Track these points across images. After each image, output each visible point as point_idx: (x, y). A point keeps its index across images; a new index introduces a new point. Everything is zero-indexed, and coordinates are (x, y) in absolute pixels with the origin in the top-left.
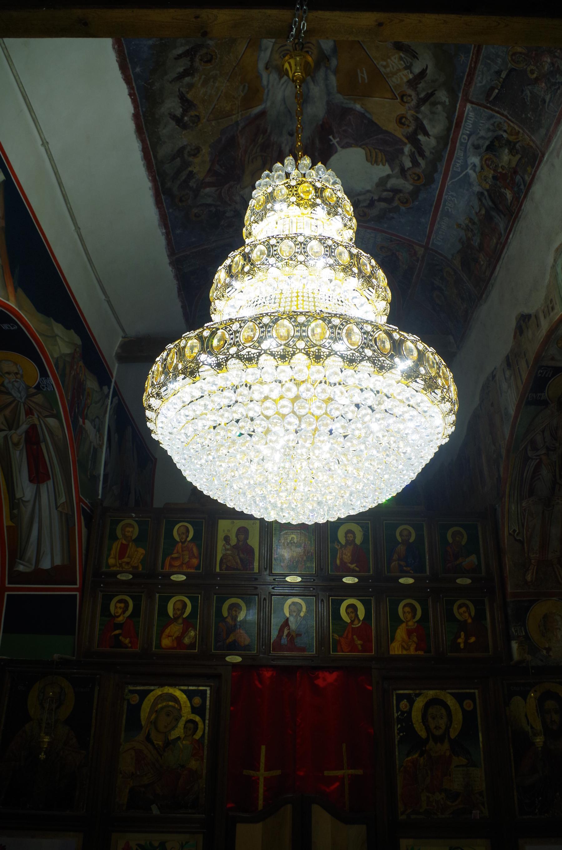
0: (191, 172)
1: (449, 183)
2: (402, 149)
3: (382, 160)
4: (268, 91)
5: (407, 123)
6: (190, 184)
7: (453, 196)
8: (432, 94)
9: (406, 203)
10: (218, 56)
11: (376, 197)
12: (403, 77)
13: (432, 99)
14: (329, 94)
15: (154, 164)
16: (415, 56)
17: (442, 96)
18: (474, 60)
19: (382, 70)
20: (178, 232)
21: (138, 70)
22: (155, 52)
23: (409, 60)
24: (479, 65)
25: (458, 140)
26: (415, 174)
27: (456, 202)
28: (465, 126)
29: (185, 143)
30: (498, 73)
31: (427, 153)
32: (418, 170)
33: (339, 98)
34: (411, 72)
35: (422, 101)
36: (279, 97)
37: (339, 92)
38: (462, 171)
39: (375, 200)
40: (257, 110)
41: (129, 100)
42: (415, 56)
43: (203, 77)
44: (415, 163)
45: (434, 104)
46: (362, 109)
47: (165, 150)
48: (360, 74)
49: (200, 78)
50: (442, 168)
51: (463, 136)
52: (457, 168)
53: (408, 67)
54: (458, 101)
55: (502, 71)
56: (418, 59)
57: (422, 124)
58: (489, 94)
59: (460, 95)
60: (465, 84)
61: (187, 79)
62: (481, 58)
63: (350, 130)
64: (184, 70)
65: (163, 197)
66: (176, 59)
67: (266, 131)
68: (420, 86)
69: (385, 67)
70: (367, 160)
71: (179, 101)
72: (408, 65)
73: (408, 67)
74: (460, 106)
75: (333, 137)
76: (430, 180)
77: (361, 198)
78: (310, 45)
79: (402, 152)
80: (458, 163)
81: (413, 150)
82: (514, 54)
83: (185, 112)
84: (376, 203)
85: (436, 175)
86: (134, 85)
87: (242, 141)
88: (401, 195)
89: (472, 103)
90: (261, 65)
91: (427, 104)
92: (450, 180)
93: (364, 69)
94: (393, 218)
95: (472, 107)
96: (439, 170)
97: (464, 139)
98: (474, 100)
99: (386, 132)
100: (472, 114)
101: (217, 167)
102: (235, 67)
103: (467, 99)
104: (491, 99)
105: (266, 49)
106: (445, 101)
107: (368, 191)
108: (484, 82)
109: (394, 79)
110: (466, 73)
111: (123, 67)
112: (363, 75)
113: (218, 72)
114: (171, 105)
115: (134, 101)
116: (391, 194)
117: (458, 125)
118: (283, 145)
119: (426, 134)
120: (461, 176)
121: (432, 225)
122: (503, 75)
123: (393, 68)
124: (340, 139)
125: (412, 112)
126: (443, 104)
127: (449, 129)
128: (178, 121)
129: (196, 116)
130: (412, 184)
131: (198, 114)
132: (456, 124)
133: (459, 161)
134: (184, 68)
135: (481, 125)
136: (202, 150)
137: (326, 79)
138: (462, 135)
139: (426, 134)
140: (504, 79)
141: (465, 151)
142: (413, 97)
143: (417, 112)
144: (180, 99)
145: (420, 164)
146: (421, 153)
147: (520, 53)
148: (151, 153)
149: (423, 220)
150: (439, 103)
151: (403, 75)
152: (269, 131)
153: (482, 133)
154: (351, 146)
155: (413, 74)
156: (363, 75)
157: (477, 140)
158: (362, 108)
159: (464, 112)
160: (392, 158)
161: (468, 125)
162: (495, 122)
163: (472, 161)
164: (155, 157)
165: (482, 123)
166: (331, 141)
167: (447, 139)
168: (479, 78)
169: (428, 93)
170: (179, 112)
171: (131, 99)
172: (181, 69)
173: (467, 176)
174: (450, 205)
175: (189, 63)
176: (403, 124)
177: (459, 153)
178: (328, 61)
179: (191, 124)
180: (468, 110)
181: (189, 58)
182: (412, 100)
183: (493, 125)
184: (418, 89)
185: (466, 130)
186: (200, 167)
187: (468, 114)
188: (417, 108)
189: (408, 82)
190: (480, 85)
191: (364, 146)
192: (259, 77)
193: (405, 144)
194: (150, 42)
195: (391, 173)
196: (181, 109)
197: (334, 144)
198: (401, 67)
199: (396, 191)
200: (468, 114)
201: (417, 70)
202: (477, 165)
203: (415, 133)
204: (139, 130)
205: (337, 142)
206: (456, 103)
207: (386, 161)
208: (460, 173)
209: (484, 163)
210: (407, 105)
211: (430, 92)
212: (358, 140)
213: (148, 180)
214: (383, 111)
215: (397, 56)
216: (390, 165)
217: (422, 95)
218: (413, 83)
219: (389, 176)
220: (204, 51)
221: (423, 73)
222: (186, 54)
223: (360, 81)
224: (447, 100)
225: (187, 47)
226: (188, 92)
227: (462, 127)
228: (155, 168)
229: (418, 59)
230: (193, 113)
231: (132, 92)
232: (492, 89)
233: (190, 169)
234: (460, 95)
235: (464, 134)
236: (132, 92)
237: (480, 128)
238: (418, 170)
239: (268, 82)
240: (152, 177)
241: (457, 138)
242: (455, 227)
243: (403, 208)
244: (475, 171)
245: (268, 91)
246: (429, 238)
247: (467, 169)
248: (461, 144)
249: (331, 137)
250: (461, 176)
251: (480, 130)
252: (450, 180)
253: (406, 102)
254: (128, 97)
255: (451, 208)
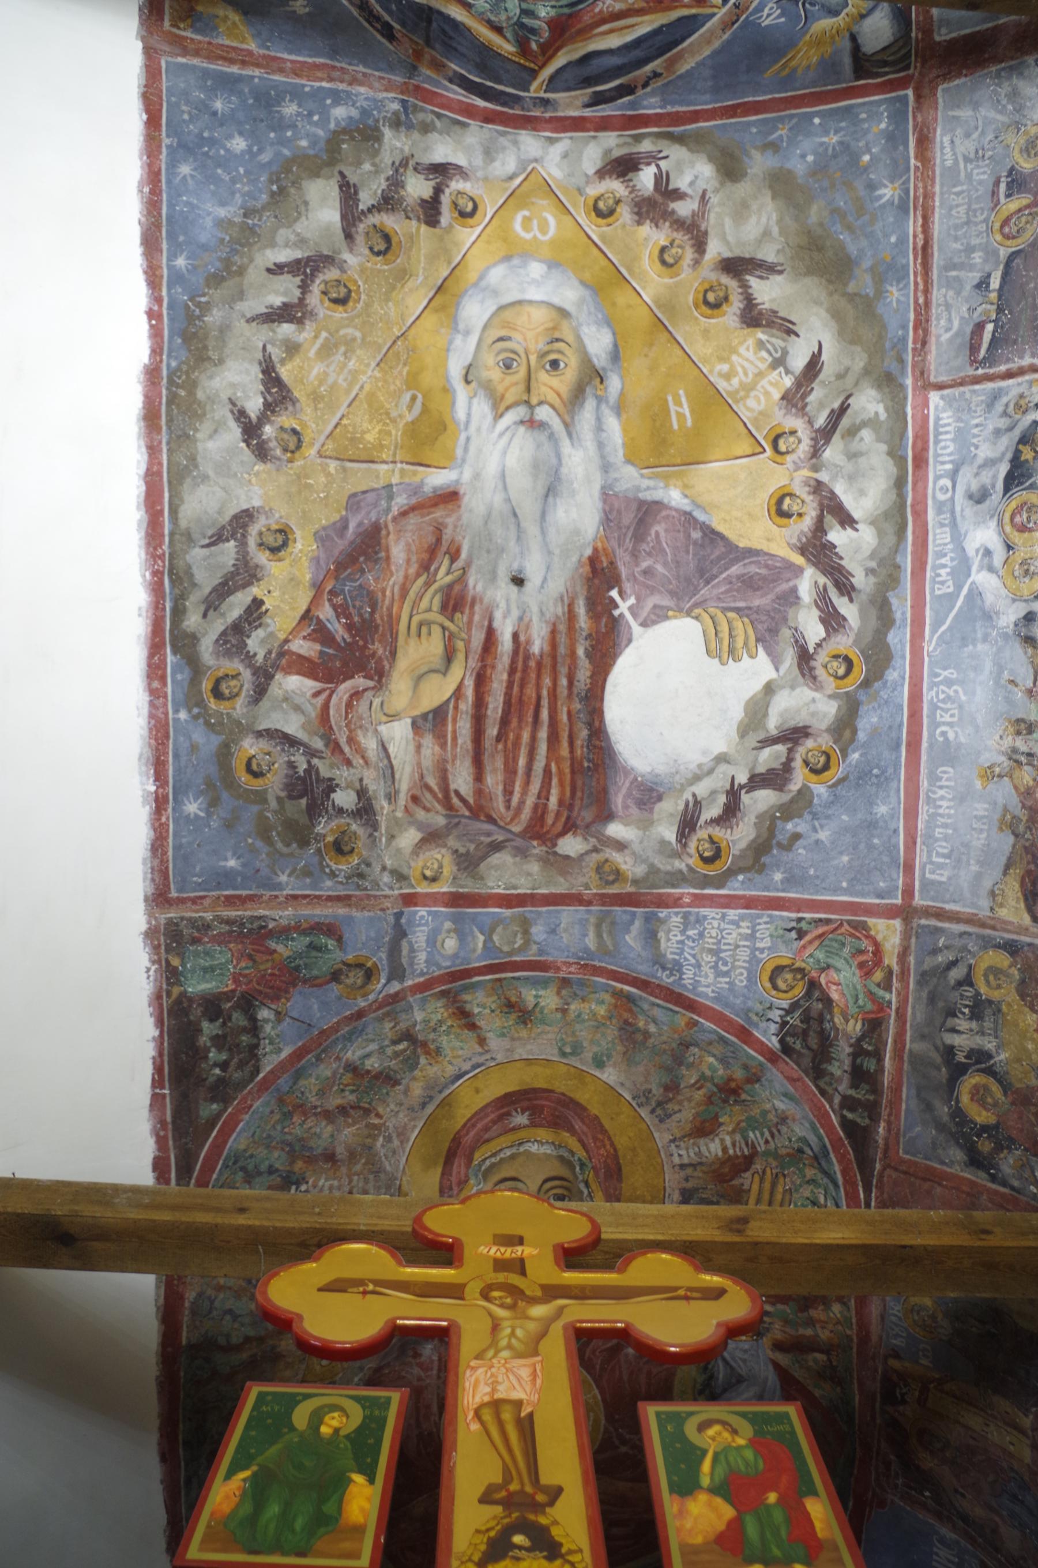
0: (257, 603)
1: (930, 646)
2: (794, 590)
3: (746, 644)
4: (468, 439)
5: (795, 508)
6: (249, 642)
7: (949, 682)
8: (843, 409)
9: (826, 767)
10: (363, 297)
11: (742, 778)
12: (771, 389)
13: (845, 422)
14: (606, 467)
15: (166, 532)
16: (789, 330)
17: (869, 403)
18: (921, 287)
19: (722, 385)
20: (192, 808)
21: (181, 262)
22: (227, 238)
23: (779, 343)
24: (935, 292)
25: (930, 502)
26: (836, 657)
27: (963, 698)
28: (937, 455)
29: (257, 503)
30: (983, 285)
31: (859, 579)
32: (843, 643)
33: (630, 478)
34: (788, 372)
35: (826, 434)
36: (492, 468)
37: (629, 461)
38: (959, 587)
39: (741, 787)
40: (438, 479)
41: (143, 326)
42: (789, 330)
43: (324, 334)
44: (832, 620)
45: (852, 432)
46: (686, 501)
47: (203, 503)
48: (673, 408)
49: (316, 337)
50: (902, 606)
51: (937, 484)
52: (943, 583)
53: (779, 362)
54: (905, 398)
55: (989, 276)
56: (798, 335)
57: (833, 496)
58: (974, 349)
59: (909, 382)
60: (914, 350)
61: (286, 329)
62: (935, 277)
63: (660, 568)
64: (285, 304)
65: (170, 658)
66: (269, 270)
67: (458, 551)
68: (811, 398)
69: (727, 377)
70: (708, 652)
71: (261, 376)
72: (778, 355)
73: (779, 362)
74: (913, 408)
75: (621, 593)
76: (878, 656)
77: (701, 789)
78: (561, 345)
79: (791, 598)
80: (944, 566)
81: (822, 580)
82: (1006, 222)
83: (270, 408)
84: (745, 798)
85: (892, 638)
86: (164, 293)
87: (398, 552)
88: (810, 743)
89: (940, 387)
90: (455, 368)
91: (836, 438)
92: (934, 632)
93: (681, 392)
94: (796, 837)
95: (942, 398)
96: (898, 616)
97: (944, 490)
98: (943, 378)
99: (750, 552)
100: (947, 417)
101: (326, 612)
102: (398, 338)
103: (926, 385)
104: (983, 352)
105: (467, 333)
106: (877, 413)
107: (722, 759)
108: (956, 324)
109: (751, 403)
110: (911, 325)
111: (150, 243)
112: (681, 410)
113: (358, 334)
114: (236, 380)
115: (156, 333)
116: (781, 748)
117: (921, 461)
118: (498, 615)
119: (847, 520)
120: (959, 603)
121: (911, 813)
122: (995, 283)
123: (746, 374)
124: (638, 599)
125: (806, 473)
126: (872, 423)
127: (900, 483)
128: (251, 431)
129: (294, 431)
130: (832, 697)
131: (298, 428)
132: (915, 458)
133: (943, 561)
134: (285, 300)
135: (975, 431)
136: (295, 541)
137: (599, 427)
138: (935, 483)
139: (847, 520)
140: (1001, 290)
141: (954, 524)
142: (799, 434)
143: (815, 469)
144: (263, 372)
145: (845, 619)
146: (846, 588)
147: (1020, 210)
148: (166, 495)
149: (882, 809)
150: (864, 424)
151: (771, 384)
152: (464, 555)
153: (985, 452)
154: (667, 618)
155: (792, 373)
156: (681, 410)
157: (977, 474)
158: (686, 496)
159: (926, 418)
160: (770, 628)
161: (944, 448)
162: (1007, 405)
163: (977, 545)
164: (174, 511)
165: (977, 426)
166: (616, 606)
167: (904, 515)
168: (943, 322)
169: (833, 411)
170: (254, 405)
171: (151, 326)
172: (278, 301)
173: (975, 594)
174: (947, 718)
175: (297, 293)
176: (787, 515)
177: (939, 537)
178: (602, 382)
179: (278, 452)
180: (936, 408)
181: (297, 280)
182: (800, 441)
183: (1005, 414)
184: (808, 409)
185: (943, 463)
186: (286, 589)
187: (938, 419)
188: (816, 453)
189: (783, 398)
190: (948, 335)
191: (697, 611)
192: (447, 390)
193: (799, 571)
194: (222, 212)
195: (773, 675)
196: (261, 400)
197: (621, 615)
198: (763, 366)
199: (794, 735)
200: (938, 419)
201: (799, 362)
202: (991, 547)
203: (820, 528)
204: (150, 417)
205: (630, 608)
206: (904, 406)
207: (758, 640)
208: (952, 597)
209: (1008, 528)
210: (789, 458)
211: (836, 405)
212: (684, 595)
213: (141, 580)
214: (735, 495)
215: (751, 342)
216: (769, 653)
217: (821, 421)
218: (794, 399)
219: (769, 689)
220: (332, 274)
221: (814, 366)
222: (294, 267)
223: (676, 426)
224: (881, 409)
225: (298, 254)
226: (283, 362)
227: (931, 461)
228: (165, 547)
229: (798, 335)
230: (285, 420)
231: (156, 308)
232: (980, 327)
233: (255, 591)
234: (909, 382)
235: (940, 477)
236: (156, 308)
237: (975, 441)
238: (843, 643)
239: (469, 415)
240: (155, 573)
241: (925, 496)
242: (978, 784)
243: (820, 790)
244: (991, 569)
245: (468, 439)
246: (909, 868)
247: (969, 575)
248: (940, 507)
249: (614, 593)
250: (959, 603)
251: (977, 447)
252: (934, 632)
253: (788, 452)
254: (145, 318)
255: (950, 725)
